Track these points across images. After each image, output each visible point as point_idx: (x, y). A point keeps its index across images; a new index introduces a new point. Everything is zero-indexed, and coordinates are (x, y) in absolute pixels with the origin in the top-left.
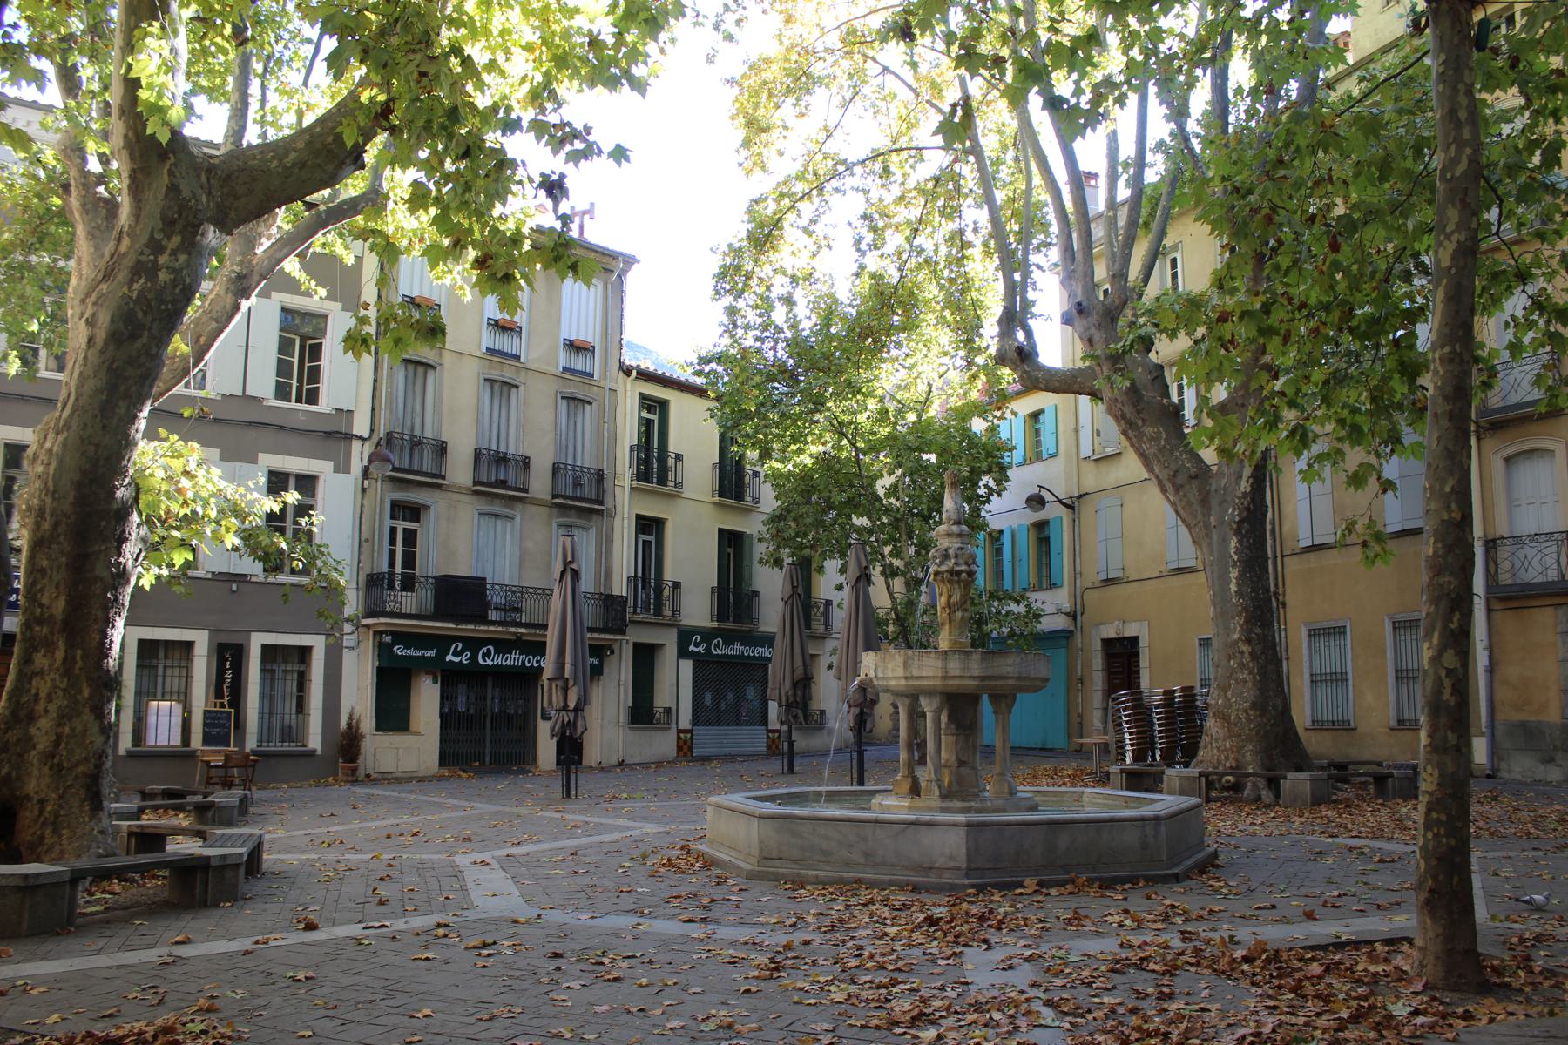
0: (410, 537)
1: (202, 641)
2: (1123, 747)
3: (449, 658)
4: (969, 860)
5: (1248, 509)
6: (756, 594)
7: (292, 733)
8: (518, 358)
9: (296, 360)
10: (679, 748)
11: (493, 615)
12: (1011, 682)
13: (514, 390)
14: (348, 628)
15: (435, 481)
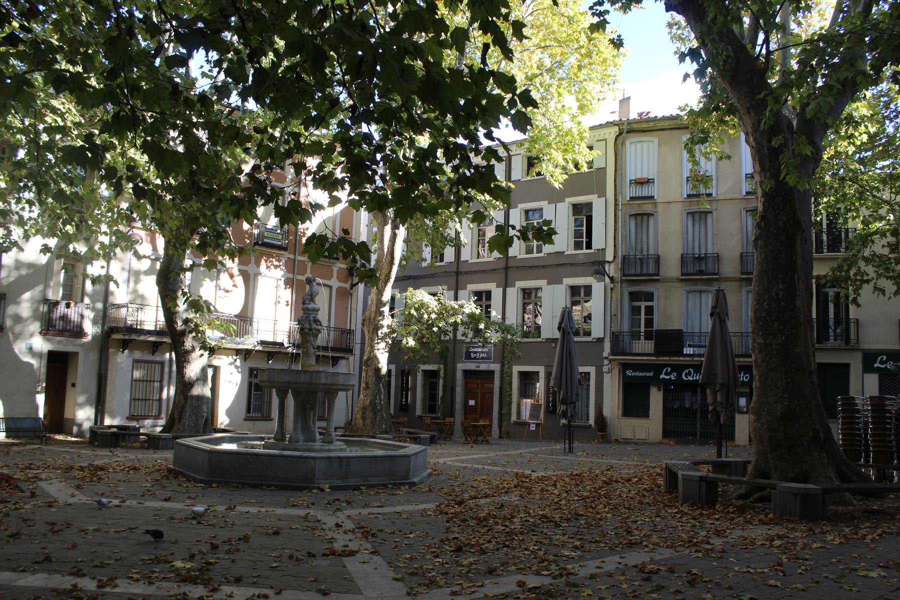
0: (650, 311)
1: (541, 370)
3: (662, 376)
8: (652, 197)
9: (584, 228)
11: (687, 351)
13: (710, 215)
14: (606, 362)
15: (655, 277)
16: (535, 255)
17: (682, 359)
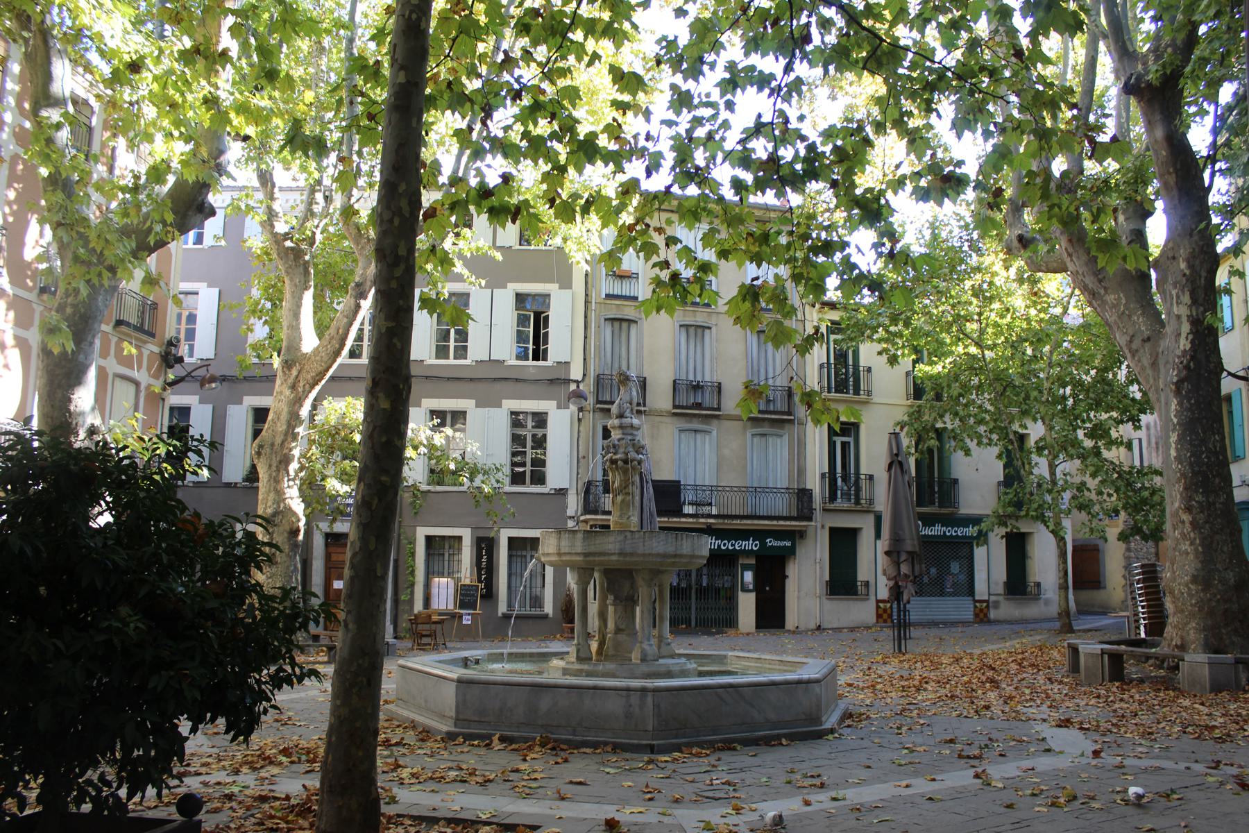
1: (467, 535)
2: (1137, 621)
4: (457, 712)
5: (1187, 367)
6: (956, 481)
7: (537, 601)
9: (531, 329)
10: (879, 616)
11: (688, 509)
12: (614, 558)
13: (707, 331)
16: (452, 361)
17: (683, 520)
